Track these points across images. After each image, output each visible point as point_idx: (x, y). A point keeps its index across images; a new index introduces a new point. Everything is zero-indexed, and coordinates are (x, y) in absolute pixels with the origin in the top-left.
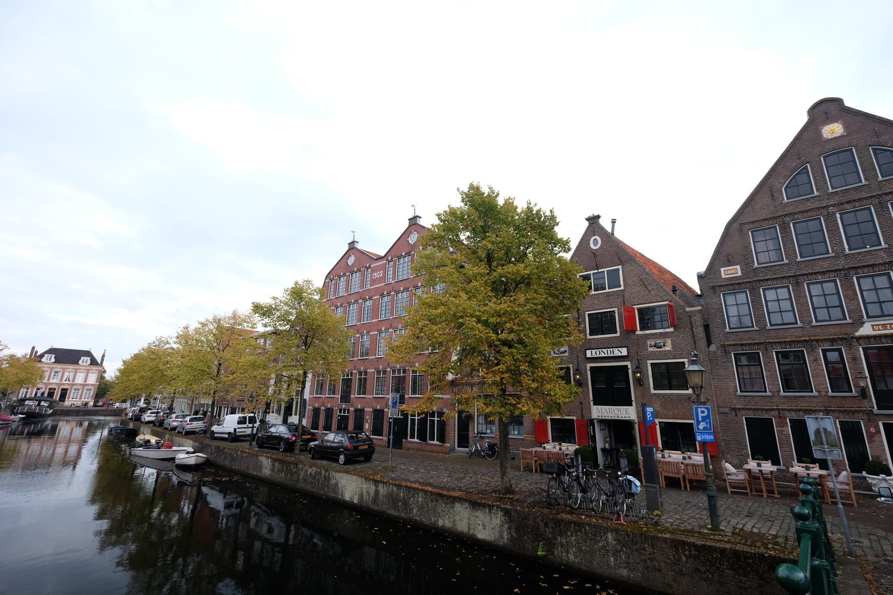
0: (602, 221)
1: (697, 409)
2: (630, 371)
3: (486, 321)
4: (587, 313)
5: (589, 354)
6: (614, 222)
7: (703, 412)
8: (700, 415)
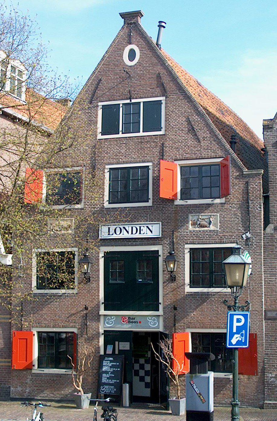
0: (142, 22)
1: (232, 316)
2: (161, 259)
3: (53, 194)
4: (150, 203)
5: (104, 233)
6: (161, 25)
7: (239, 321)
8: (235, 324)
